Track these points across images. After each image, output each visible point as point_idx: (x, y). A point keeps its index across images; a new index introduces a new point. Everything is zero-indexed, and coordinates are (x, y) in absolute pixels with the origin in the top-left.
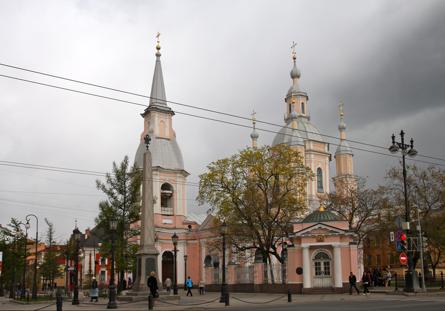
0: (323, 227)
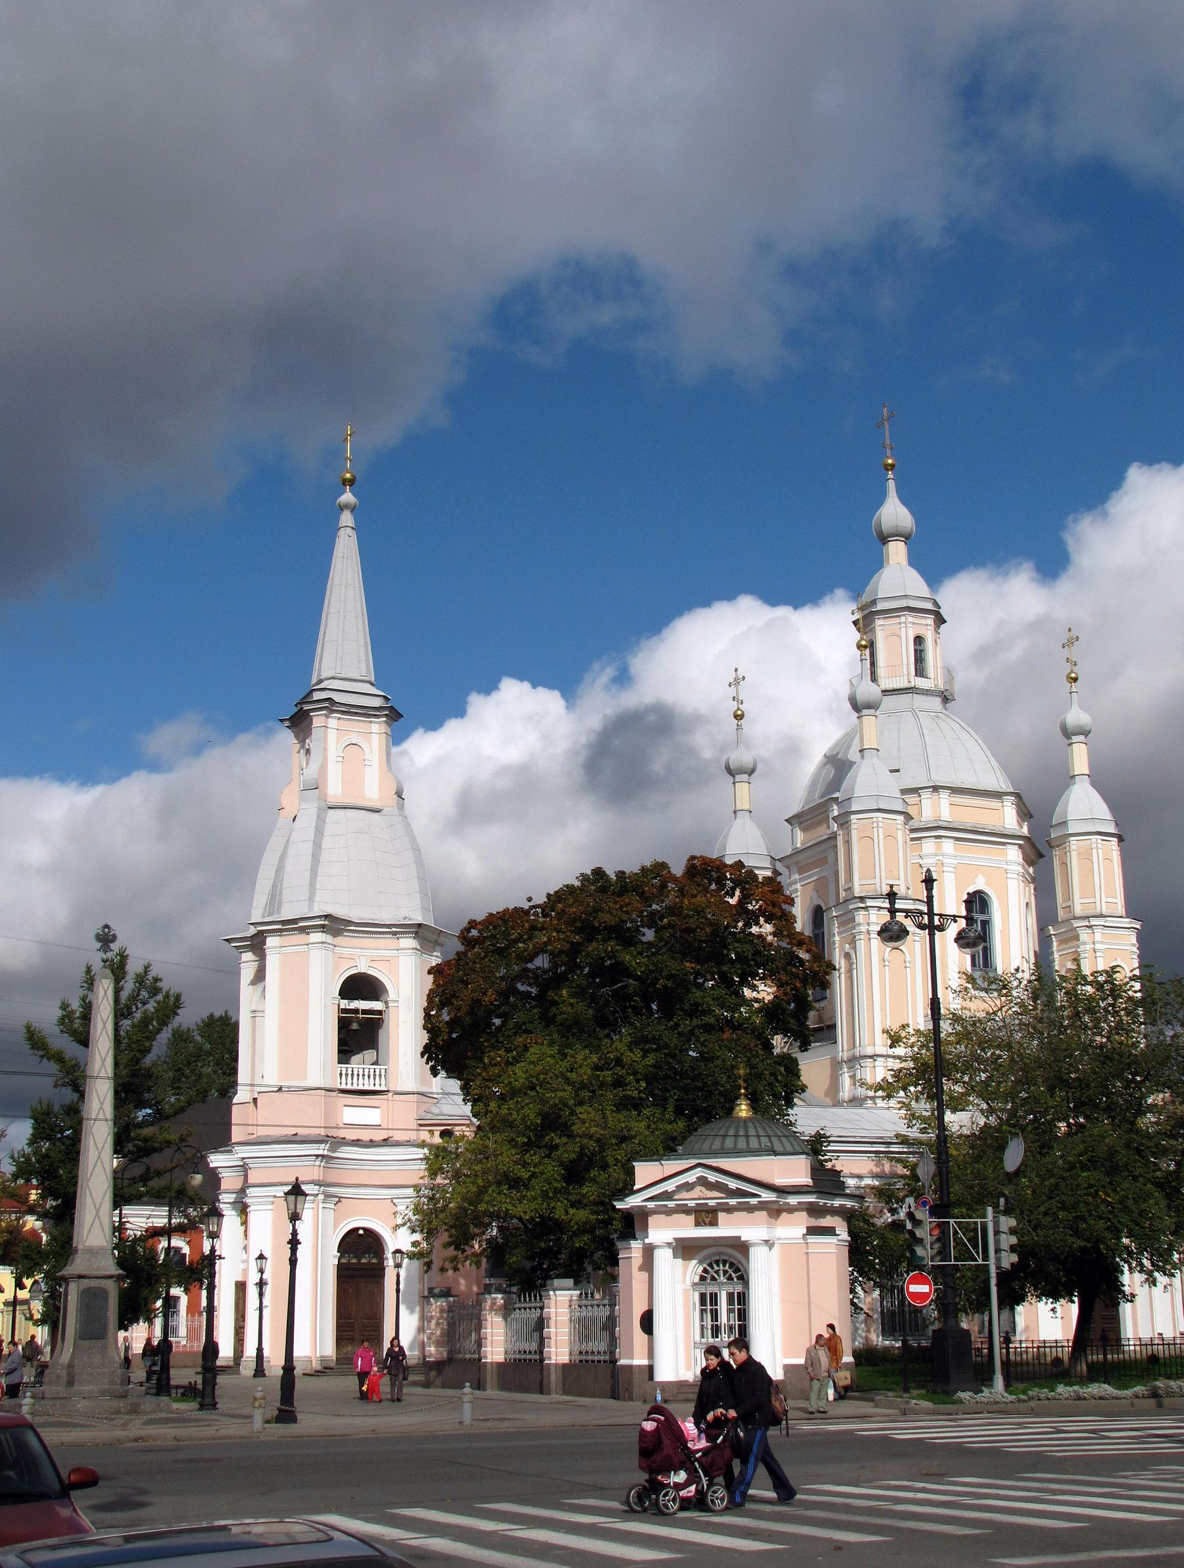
0: (712, 1177)
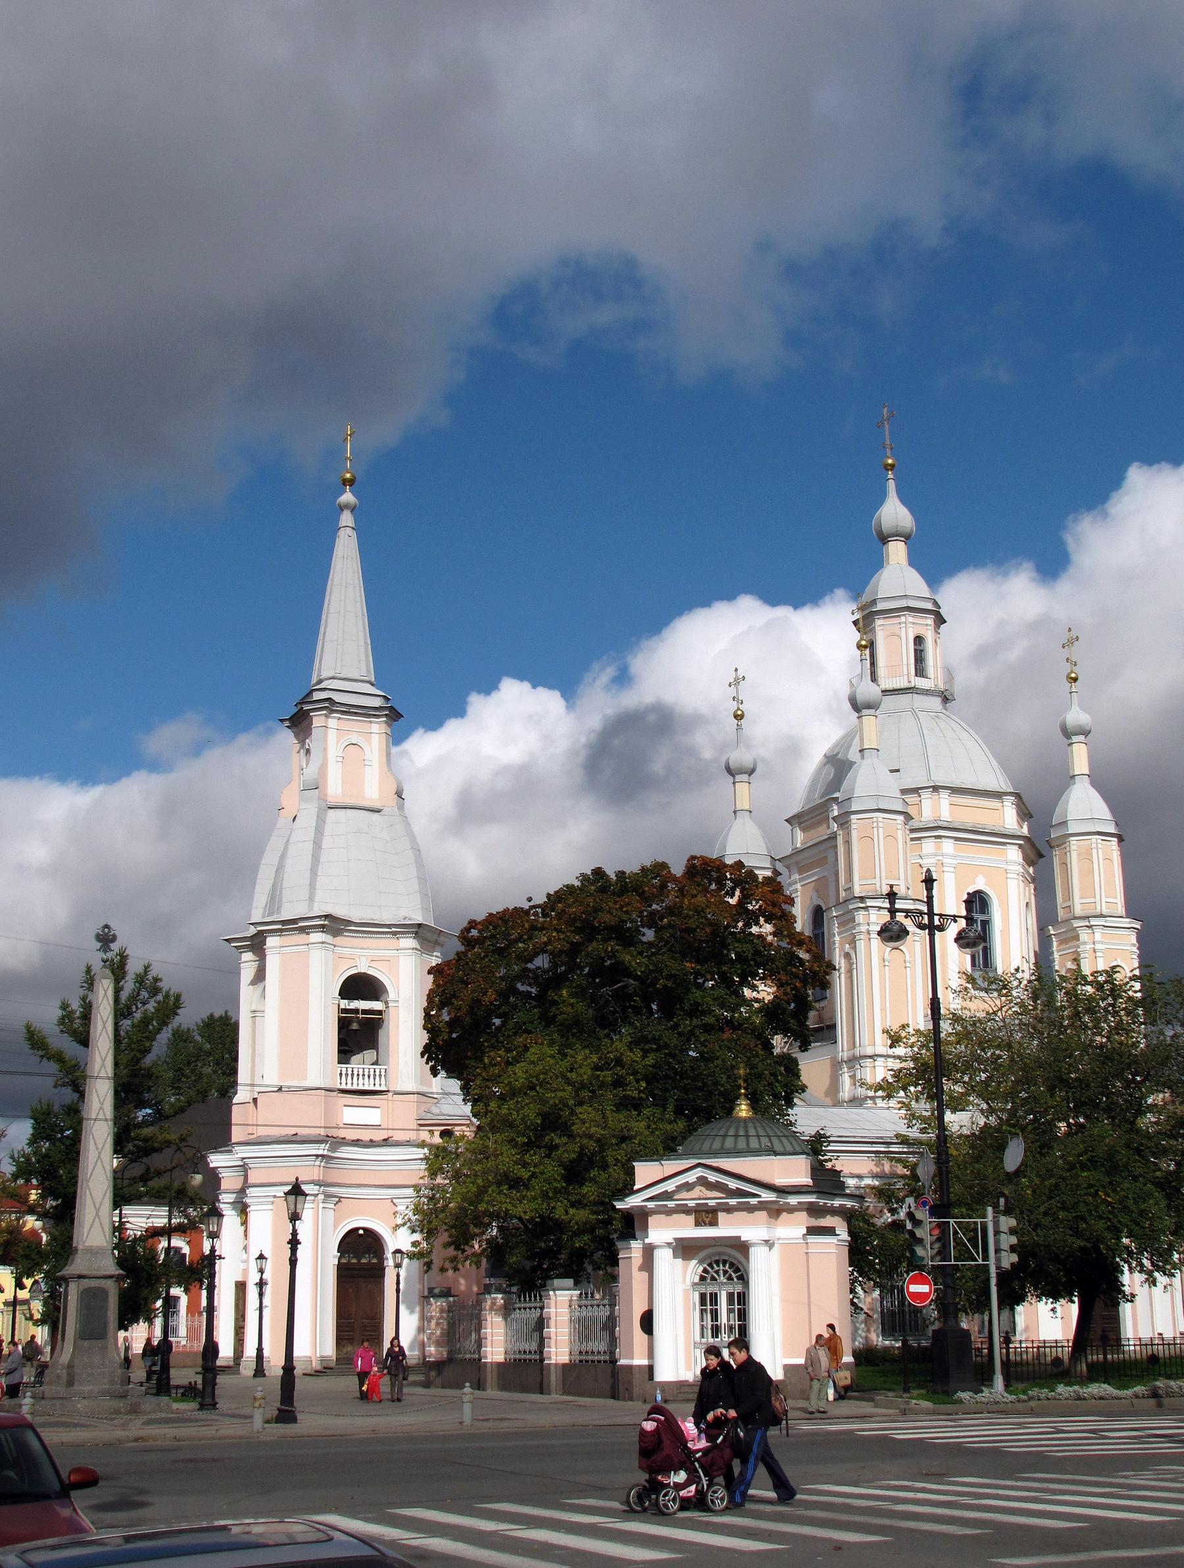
0: (712, 1177)
